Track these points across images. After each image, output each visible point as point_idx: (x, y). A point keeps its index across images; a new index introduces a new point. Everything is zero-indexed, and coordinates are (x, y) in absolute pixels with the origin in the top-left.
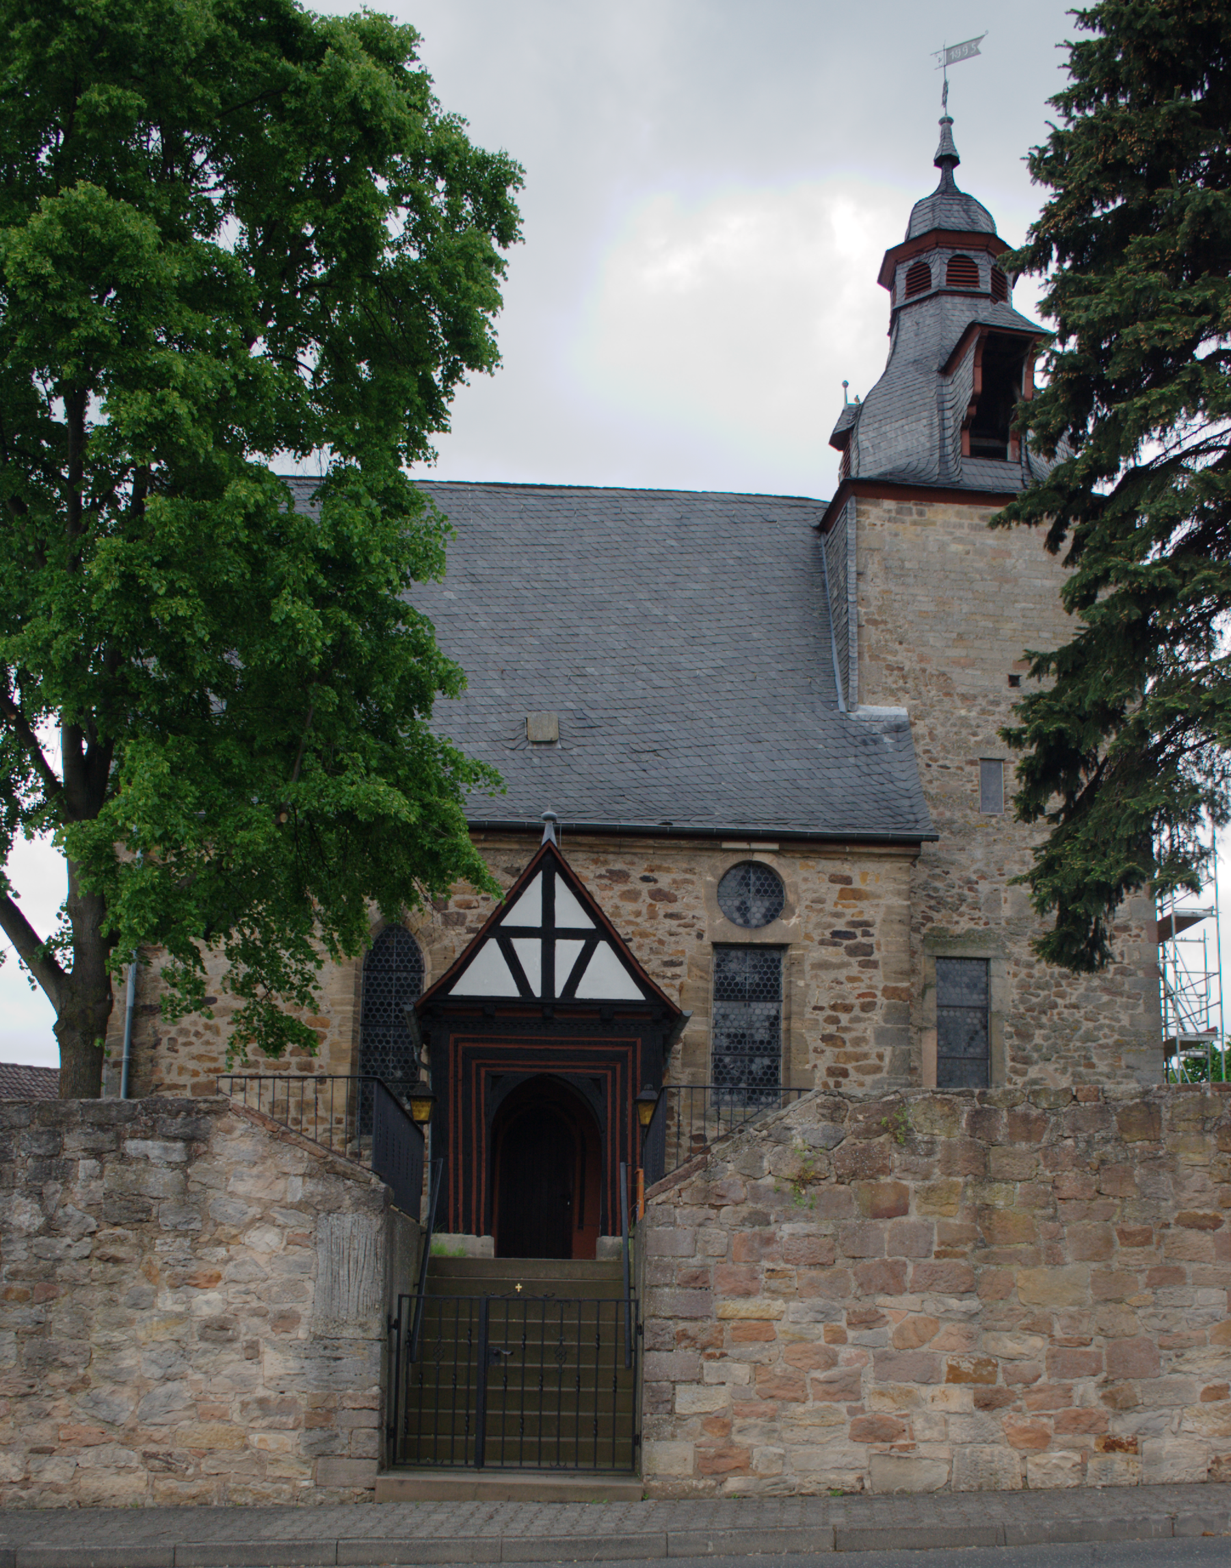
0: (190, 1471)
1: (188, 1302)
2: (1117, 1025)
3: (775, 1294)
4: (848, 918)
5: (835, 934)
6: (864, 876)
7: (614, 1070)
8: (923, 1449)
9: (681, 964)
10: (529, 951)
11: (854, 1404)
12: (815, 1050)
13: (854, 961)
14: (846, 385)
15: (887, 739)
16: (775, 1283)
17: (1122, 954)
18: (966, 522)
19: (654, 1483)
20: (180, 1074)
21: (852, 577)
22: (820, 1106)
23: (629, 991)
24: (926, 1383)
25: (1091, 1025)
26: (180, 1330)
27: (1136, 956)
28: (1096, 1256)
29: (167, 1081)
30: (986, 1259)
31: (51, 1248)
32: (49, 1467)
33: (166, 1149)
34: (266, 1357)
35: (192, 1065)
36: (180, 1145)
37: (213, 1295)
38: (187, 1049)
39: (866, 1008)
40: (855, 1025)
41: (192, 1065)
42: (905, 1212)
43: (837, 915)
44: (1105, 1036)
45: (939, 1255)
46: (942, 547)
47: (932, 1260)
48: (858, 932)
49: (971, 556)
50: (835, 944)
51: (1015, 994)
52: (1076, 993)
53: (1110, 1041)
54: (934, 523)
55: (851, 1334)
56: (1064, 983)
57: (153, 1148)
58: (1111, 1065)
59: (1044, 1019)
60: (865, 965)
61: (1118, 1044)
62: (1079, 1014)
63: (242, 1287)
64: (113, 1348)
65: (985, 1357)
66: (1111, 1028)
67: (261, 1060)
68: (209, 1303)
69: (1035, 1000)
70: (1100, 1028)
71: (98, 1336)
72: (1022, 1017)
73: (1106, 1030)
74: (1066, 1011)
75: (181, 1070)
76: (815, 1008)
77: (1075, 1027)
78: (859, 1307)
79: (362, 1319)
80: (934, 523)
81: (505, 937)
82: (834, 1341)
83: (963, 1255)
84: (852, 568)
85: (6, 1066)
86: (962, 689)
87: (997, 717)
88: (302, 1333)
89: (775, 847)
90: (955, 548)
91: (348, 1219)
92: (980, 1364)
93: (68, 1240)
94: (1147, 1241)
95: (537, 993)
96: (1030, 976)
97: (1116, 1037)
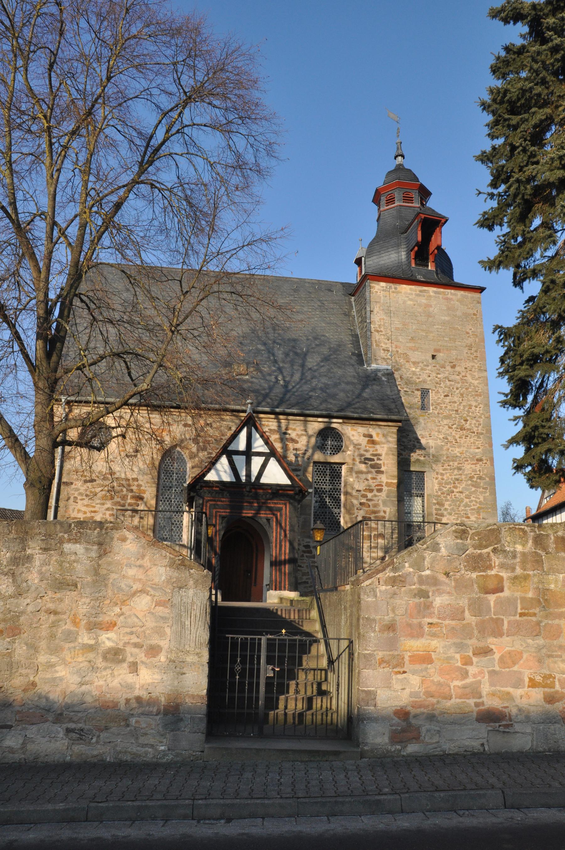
0: (94, 740)
1: (96, 638)
2: (478, 500)
3: (434, 635)
4: (371, 452)
5: (366, 459)
6: (378, 434)
8: (517, 727)
9: (300, 470)
10: (240, 461)
11: (478, 701)
12: (357, 509)
13: (373, 470)
15: (384, 379)
16: (434, 629)
17: (480, 471)
18: (414, 293)
19: (366, 748)
20: (78, 513)
21: (368, 313)
22: (455, 531)
23: (284, 480)
24: (517, 688)
25: (468, 500)
26: (91, 656)
27: (485, 471)
29: (72, 516)
30: (546, 617)
31: (17, 605)
32: (8, 737)
33: (87, 549)
34: (141, 671)
35: (84, 509)
36: (95, 547)
37: (111, 635)
38: (82, 502)
39: (380, 490)
40: (374, 498)
41: (84, 509)
42: (502, 590)
43: (366, 451)
44: (474, 505)
45: (521, 615)
46: (404, 302)
47: (518, 617)
51: (436, 487)
52: (461, 487)
55: (475, 660)
56: (456, 482)
57: (79, 548)
59: (449, 497)
61: (479, 508)
62: (462, 496)
63: (128, 630)
64: (50, 666)
65: (548, 673)
66: (475, 501)
68: (108, 639)
69: (445, 489)
70: (471, 502)
71: (42, 658)
72: (439, 496)
73: (474, 503)
74: (457, 495)
76: (357, 491)
78: (481, 644)
79: (198, 651)
81: (230, 454)
82: (466, 664)
83: (535, 615)
84: (368, 309)
86: (413, 360)
87: (427, 371)
88: (162, 658)
89: (340, 421)
90: (409, 303)
91: (191, 592)
92: (545, 677)
93: (28, 601)
95: (243, 479)
96: (443, 479)
97: (478, 505)
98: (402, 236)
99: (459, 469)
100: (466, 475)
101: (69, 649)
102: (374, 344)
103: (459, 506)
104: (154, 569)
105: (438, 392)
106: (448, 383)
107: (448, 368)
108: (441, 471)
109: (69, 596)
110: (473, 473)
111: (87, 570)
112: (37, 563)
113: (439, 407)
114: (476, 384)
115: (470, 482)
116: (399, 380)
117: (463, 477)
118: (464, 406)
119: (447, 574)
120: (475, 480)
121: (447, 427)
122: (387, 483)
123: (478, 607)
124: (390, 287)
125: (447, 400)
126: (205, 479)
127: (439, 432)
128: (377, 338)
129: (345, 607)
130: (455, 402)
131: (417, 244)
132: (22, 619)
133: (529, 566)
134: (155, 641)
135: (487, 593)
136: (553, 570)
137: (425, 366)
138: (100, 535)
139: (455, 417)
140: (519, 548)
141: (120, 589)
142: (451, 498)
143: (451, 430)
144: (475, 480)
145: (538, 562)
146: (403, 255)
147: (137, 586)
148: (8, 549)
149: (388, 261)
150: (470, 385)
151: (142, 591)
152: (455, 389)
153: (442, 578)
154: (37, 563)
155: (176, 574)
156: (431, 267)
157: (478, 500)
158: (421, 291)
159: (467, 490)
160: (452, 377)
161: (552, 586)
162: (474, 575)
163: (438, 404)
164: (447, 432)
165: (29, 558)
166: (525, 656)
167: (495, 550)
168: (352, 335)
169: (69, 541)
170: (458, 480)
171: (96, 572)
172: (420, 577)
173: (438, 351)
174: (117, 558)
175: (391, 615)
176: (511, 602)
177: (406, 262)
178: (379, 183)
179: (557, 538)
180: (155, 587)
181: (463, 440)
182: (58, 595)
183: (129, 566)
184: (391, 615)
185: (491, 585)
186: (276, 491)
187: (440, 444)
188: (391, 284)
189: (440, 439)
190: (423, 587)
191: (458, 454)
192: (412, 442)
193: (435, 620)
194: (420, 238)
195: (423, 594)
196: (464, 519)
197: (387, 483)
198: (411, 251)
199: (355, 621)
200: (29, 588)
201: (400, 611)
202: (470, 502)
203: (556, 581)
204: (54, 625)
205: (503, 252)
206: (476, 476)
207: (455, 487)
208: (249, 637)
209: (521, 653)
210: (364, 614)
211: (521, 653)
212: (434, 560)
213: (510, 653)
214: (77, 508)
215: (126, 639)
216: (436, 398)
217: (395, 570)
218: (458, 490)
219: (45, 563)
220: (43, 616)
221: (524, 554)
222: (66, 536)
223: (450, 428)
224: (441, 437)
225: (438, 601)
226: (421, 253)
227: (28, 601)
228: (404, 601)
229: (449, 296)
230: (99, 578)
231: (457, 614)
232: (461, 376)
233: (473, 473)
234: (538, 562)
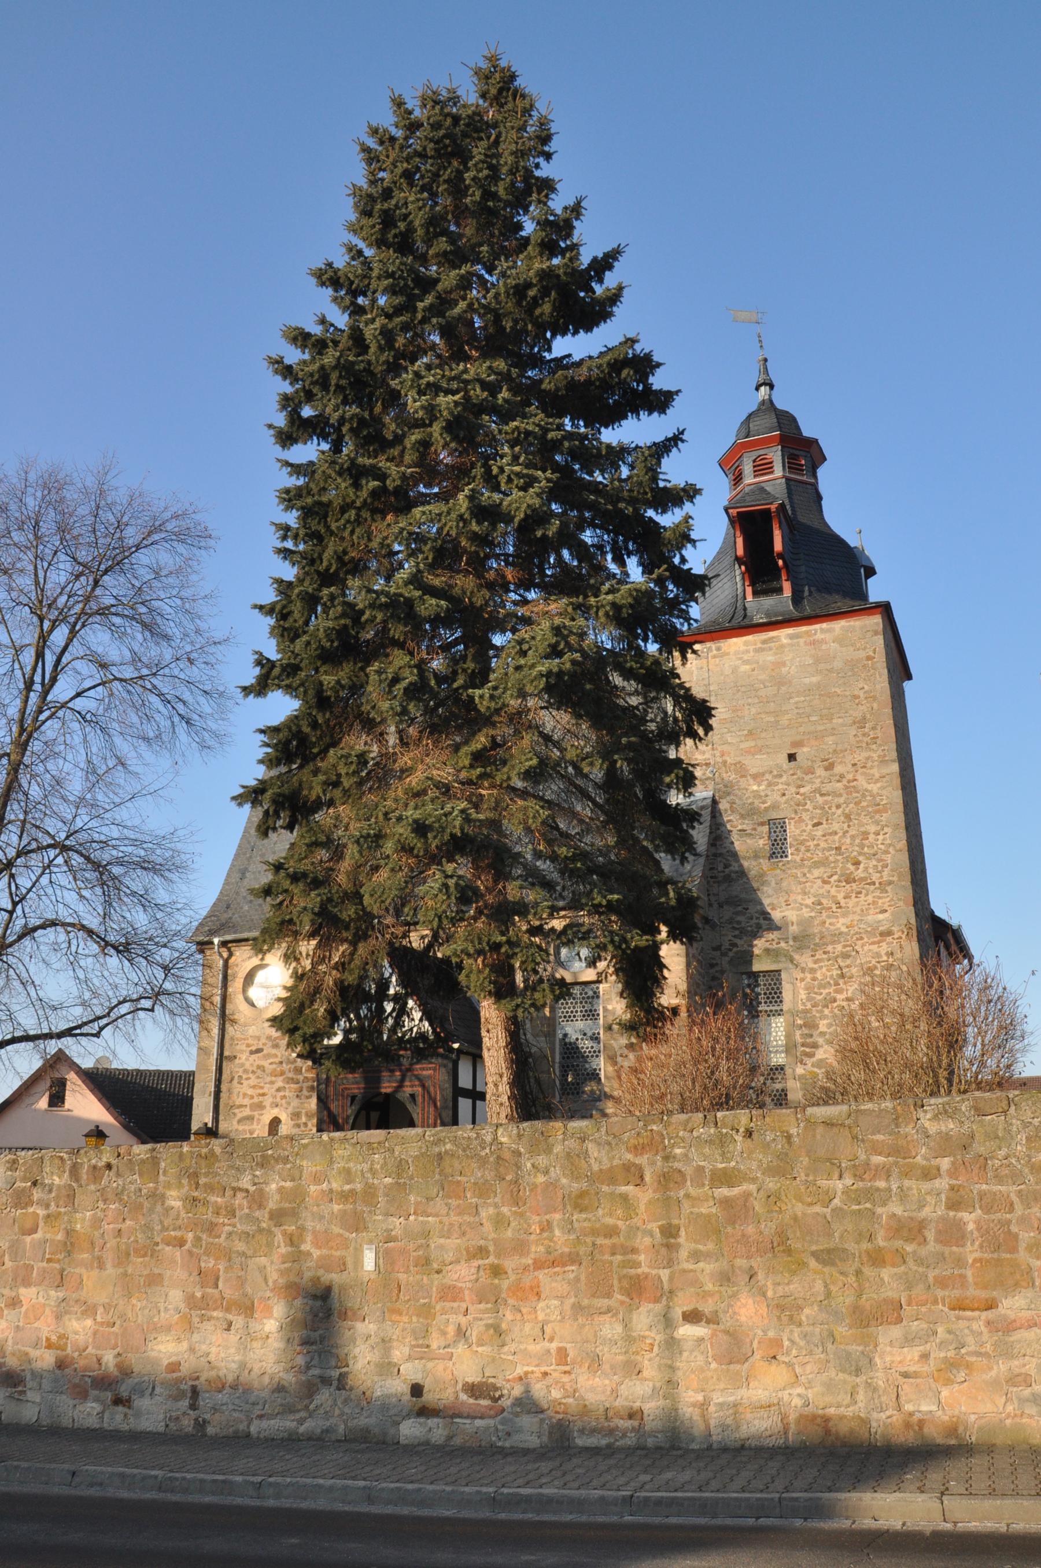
46: (735, 670)
51: (803, 995)
54: (728, 654)
56: (841, 981)
59: (826, 1011)
86: (753, 771)
96: (814, 979)
106: (820, 800)
107: (820, 772)
108: (811, 965)
113: (803, 848)
114: (875, 791)
118: (853, 837)
120: (877, 972)
121: (819, 881)
125: (819, 832)
137: (776, 777)
140: (57, 1180)
143: (827, 887)
144: (877, 972)
145: (71, 1196)
152: (834, 809)
158: (764, 642)
163: (802, 843)
164: (821, 891)
185: (28, 1225)
187: (806, 915)
189: (807, 906)
191: (844, 929)
192: (755, 921)
207: (839, 991)
216: (798, 832)
223: (825, 882)
224: (809, 902)
229: (819, 636)
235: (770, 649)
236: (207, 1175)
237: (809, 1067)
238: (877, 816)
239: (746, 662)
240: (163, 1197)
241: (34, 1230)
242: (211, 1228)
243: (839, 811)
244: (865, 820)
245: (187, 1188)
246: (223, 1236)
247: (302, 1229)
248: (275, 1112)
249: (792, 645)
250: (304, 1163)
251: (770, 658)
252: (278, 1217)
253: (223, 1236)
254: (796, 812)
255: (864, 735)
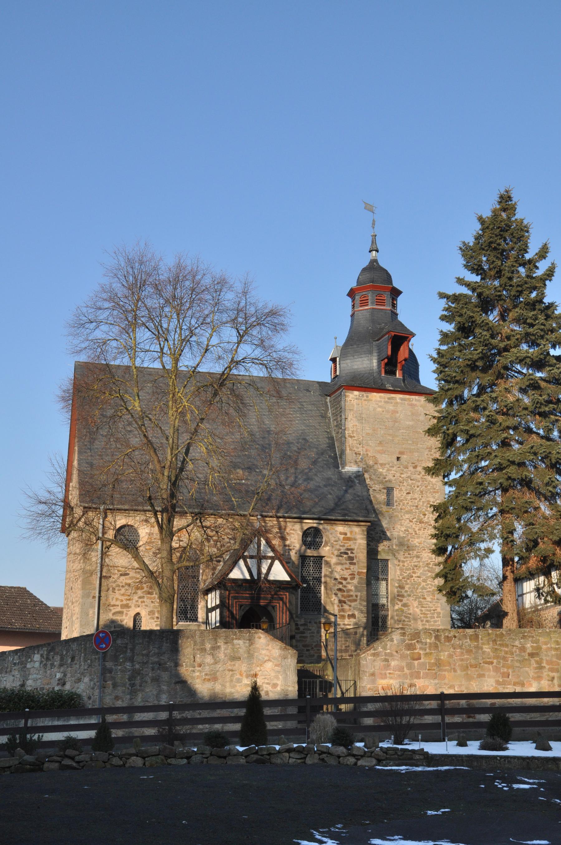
2: (433, 584)
3: (391, 678)
7: (279, 603)
13: (348, 562)
14: (336, 338)
18: (383, 400)
21: (343, 421)
22: (400, 633)
25: (424, 584)
28: (465, 670)
29: (112, 603)
30: (439, 671)
31: (215, 668)
33: (244, 643)
36: (248, 641)
42: (420, 659)
44: (430, 588)
45: (428, 670)
46: (375, 409)
47: (427, 671)
48: (349, 552)
49: (384, 413)
50: (341, 556)
51: (398, 573)
52: (419, 572)
53: (431, 590)
54: (372, 400)
56: (415, 568)
57: (241, 642)
58: (432, 599)
59: (408, 581)
60: (351, 564)
62: (420, 580)
66: (431, 584)
67: (145, 596)
69: (405, 575)
73: (430, 586)
74: (416, 579)
75: (117, 599)
77: (419, 584)
80: (372, 400)
83: (434, 670)
84: (343, 417)
85: (3, 587)
86: (381, 462)
90: (379, 409)
91: (289, 660)
93: (220, 666)
94: (476, 667)
95: (256, 578)
96: (404, 566)
98: (374, 343)
99: (418, 557)
100: (424, 562)
101: (239, 686)
102: (348, 449)
103: (417, 589)
104: (273, 650)
105: (401, 490)
106: (410, 482)
107: (411, 468)
108: (402, 559)
109: (237, 663)
110: (429, 561)
111: (245, 652)
112: (223, 649)
113: (401, 504)
114: (434, 482)
115: (426, 568)
116: (369, 480)
117: (421, 564)
118: (423, 502)
119: (397, 652)
120: (431, 566)
121: (408, 520)
122: (358, 572)
123: (410, 666)
124: (363, 396)
125: (409, 497)
126: (550, 742)
127: (401, 525)
128: (351, 443)
129: (351, 667)
130: (416, 499)
131: (387, 358)
132: (218, 673)
133: (432, 648)
134: (275, 681)
135: (414, 660)
136: (443, 650)
137: (391, 467)
138: (249, 636)
139: (416, 512)
140: (428, 641)
141: (259, 659)
142: (411, 582)
143: (411, 523)
144: (431, 566)
145: (436, 647)
146: (375, 363)
147: (266, 658)
148: (209, 643)
149: (361, 366)
150: (429, 483)
151: (269, 660)
152: (416, 487)
153: (395, 653)
154: (223, 649)
155: (283, 653)
156: (399, 375)
157: (433, 584)
158: (389, 399)
159: (424, 575)
160: (413, 477)
161: (442, 658)
162: (408, 652)
163: (401, 501)
164: (408, 525)
165: (219, 647)
166: (430, 687)
167: (418, 642)
168: (328, 438)
169: (236, 639)
170: (416, 566)
171: (249, 652)
172: (385, 653)
173: (402, 453)
174: (257, 646)
175: (373, 669)
176: (424, 664)
177: (377, 370)
178: (354, 284)
179: (445, 636)
180: (274, 658)
181: (421, 532)
182: (233, 663)
183: (263, 649)
184: (373, 669)
185: (416, 657)
186: (279, 584)
187: (402, 535)
188: (363, 393)
189: (402, 531)
190: (387, 657)
191: (417, 544)
192: (378, 535)
193: (391, 672)
194: (390, 353)
195: (387, 660)
196: (421, 600)
197: (358, 572)
198: (382, 360)
199: (357, 672)
200: (220, 660)
201: (377, 668)
202: (426, 585)
203: (444, 655)
204: (232, 676)
205: (436, 465)
206: (432, 563)
207: (414, 573)
208: (312, 680)
209: (428, 686)
210: (362, 669)
211: (428, 686)
212: (391, 645)
213: (423, 686)
214: (115, 597)
215: (263, 681)
216: (399, 495)
217: (375, 650)
218: (416, 575)
219: (226, 649)
220: (227, 672)
221: (430, 643)
222: (234, 637)
223: (410, 521)
224: (403, 529)
225: (393, 663)
226: (390, 365)
227: (220, 666)
228: (379, 663)
229: (414, 402)
230: (250, 655)
231: (401, 669)
232: (421, 476)
233: (429, 561)
234: (436, 647)
235: (392, 403)
236: (500, 641)
237: (400, 606)
238: (434, 494)
239: (380, 407)
240: (482, 648)
241: (420, 659)
242: (505, 659)
243: (418, 489)
244: (429, 495)
245: (491, 645)
246: (509, 661)
247: (542, 659)
248: (138, 610)
249: (402, 404)
250: (540, 638)
251: (391, 407)
252: (532, 655)
253: (509, 661)
254: (399, 486)
255: (431, 455)
